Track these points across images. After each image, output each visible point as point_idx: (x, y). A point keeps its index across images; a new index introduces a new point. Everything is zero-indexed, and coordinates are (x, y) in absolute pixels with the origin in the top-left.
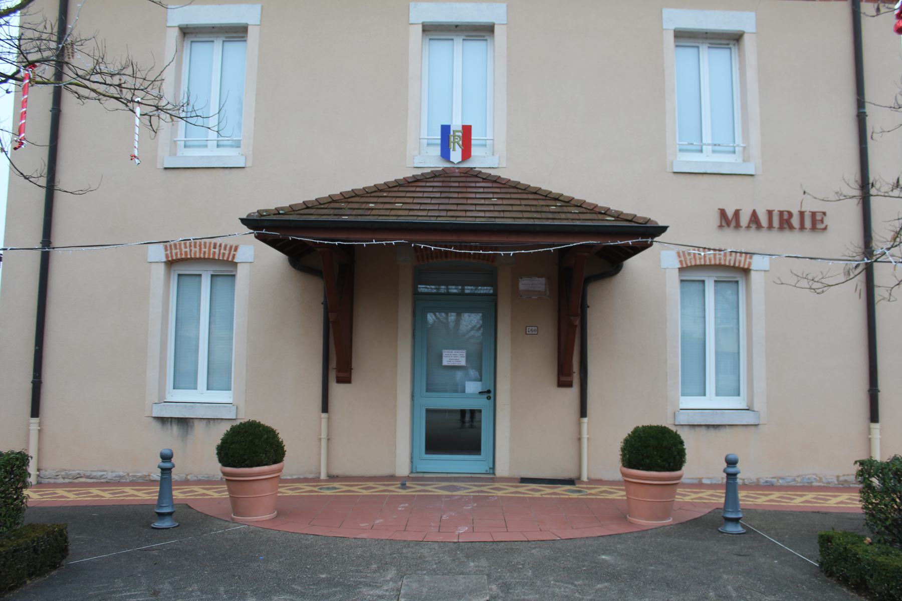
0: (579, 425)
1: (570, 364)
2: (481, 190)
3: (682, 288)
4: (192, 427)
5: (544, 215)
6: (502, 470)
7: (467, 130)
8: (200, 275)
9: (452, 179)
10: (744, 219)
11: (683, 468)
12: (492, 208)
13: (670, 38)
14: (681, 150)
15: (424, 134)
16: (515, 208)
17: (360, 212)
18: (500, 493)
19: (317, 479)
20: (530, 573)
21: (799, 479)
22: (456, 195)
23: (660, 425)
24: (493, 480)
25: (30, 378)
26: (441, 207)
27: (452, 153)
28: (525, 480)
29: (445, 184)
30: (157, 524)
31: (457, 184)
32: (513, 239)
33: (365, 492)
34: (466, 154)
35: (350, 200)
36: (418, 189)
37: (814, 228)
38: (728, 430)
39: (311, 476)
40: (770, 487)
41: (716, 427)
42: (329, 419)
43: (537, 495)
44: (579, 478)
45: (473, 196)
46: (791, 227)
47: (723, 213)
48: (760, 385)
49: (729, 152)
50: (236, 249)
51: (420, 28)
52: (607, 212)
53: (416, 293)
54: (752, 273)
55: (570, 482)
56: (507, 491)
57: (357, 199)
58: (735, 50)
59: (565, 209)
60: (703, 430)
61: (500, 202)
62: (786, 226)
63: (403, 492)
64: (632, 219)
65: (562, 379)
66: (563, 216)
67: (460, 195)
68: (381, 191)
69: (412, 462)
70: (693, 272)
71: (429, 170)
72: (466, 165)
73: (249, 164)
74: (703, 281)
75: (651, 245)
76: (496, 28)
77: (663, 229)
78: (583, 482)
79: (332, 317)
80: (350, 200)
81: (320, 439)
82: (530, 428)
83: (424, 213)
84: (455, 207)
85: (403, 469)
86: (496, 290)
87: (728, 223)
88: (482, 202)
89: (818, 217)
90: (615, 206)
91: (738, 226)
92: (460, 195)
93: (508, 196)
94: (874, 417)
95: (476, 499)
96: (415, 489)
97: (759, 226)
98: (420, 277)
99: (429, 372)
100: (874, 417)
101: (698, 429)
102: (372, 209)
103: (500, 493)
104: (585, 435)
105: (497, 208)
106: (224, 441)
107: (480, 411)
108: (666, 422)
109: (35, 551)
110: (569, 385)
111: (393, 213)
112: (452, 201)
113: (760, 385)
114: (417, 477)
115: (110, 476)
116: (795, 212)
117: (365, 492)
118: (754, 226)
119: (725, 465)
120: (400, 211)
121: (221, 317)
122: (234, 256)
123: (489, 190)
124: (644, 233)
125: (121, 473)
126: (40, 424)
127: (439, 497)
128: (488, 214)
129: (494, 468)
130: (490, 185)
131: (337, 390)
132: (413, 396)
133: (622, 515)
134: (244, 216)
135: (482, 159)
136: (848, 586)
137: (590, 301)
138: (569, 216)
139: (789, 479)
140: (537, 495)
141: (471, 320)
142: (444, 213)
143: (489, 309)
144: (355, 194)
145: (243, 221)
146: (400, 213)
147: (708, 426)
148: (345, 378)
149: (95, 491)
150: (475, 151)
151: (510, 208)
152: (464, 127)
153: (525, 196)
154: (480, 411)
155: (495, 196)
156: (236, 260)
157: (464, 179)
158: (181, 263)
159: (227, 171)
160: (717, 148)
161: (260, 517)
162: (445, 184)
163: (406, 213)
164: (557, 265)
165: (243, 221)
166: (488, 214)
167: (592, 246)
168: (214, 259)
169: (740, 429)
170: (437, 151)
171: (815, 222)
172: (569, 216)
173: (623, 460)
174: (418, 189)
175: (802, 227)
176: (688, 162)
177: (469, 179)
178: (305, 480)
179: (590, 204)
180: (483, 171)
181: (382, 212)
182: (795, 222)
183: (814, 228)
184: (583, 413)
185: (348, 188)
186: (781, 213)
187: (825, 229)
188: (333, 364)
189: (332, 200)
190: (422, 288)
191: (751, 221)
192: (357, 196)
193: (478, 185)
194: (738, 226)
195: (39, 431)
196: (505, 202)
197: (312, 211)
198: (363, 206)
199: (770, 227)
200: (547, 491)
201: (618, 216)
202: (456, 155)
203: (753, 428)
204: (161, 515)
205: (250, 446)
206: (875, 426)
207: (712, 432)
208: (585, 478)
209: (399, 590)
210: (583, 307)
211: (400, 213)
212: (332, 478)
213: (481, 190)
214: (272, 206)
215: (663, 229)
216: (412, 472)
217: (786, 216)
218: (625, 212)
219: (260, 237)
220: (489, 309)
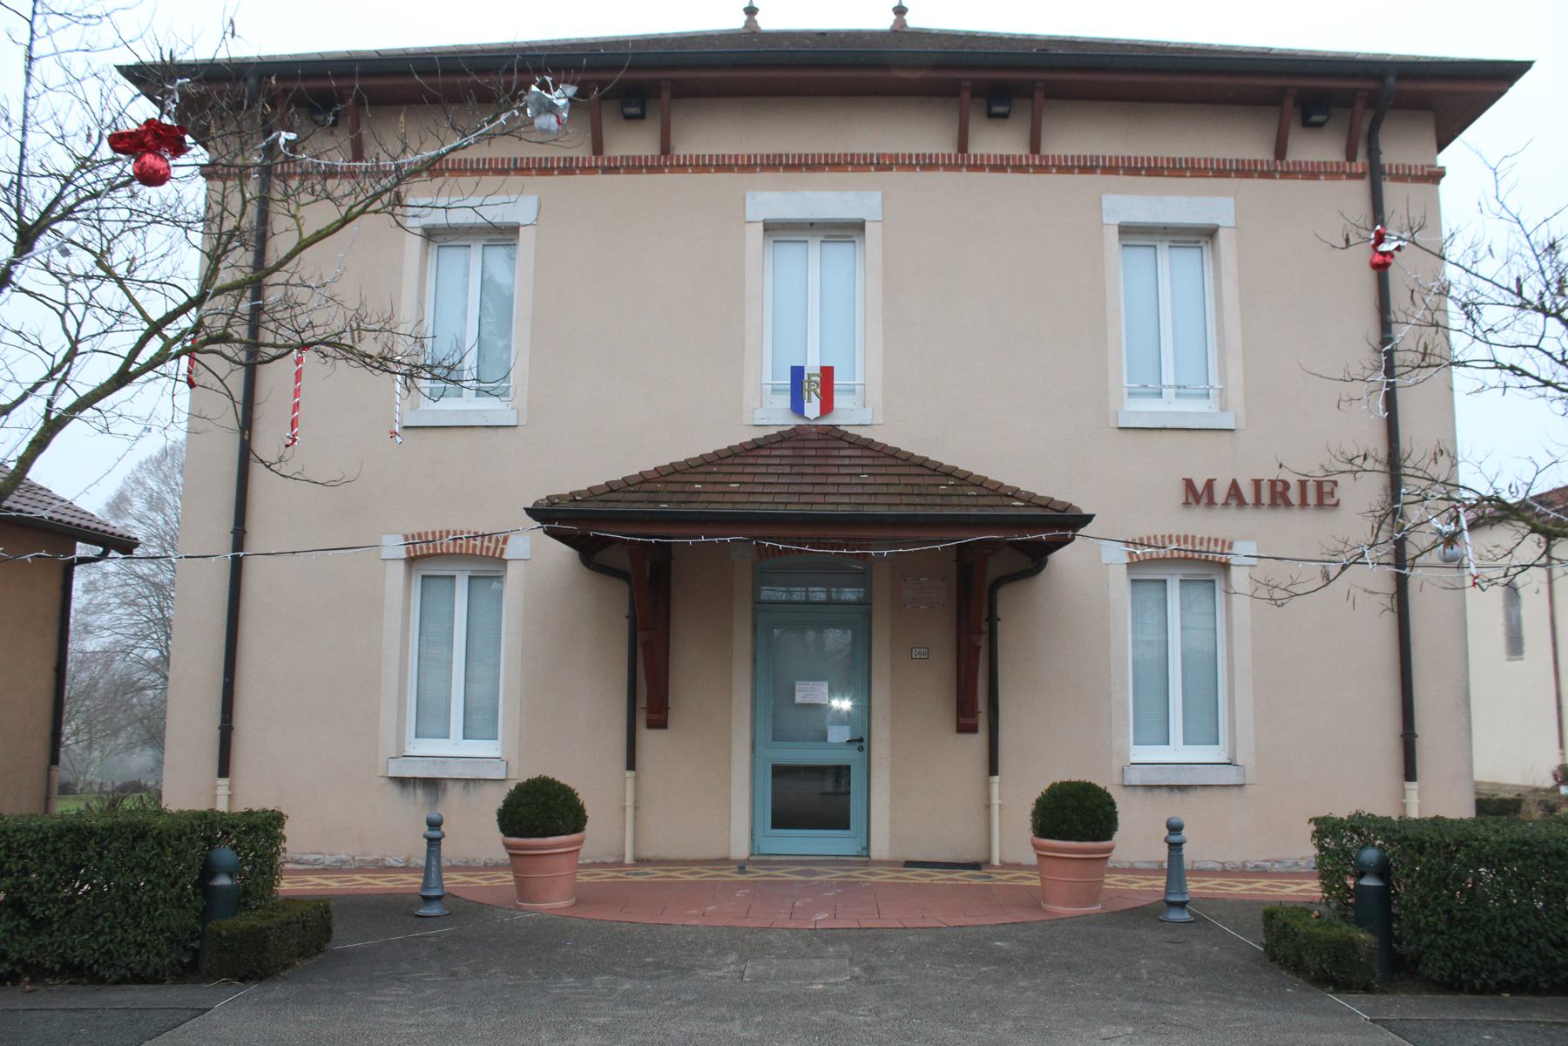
0: (988, 785)
1: (974, 703)
2: (847, 461)
3: (1134, 594)
4: (445, 790)
5: (930, 500)
6: (880, 850)
7: (827, 373)
9: (808, 444)
10: (1220, 493)
11: (1117, 836)
13: (1112, 235)
14: (1131, 394)
16: (892, 490)
18: (873, 879)
19: (620, 864)
20: (902, 957)
21: (1303, 863)
22: (811, 470)
23: (1075, 779)
24: (868, 863)
25: (217, 722)
27: (806, 404)
28: (910, 864)
29: (798, 452)
30: (422, 912)
31: (813, 453)
32: (888, 533)
36: (760, 461)
37: (1320, 504)
38: (1199, 792)
39: (612, 860)
41: (1182, 788)
42: (636, 779)
43: (926, 880)
44: (988, 863)
45: (835, 470)
46: (1288, 504)
47: (1189, 484)
49: (1200, 396)
50: (505, 541)
51: (761, 226)
52: (1015, 493)
53: (757, 602)
54: (1233, 569)
55: (975, 866)
56: (887, 876)
57: (677, 477)
59: (959, 490)
60: (1164, 793)
61: (871, 480)
62: (1279, 501)
63: (741, 877)
64: (1047, 503)
65: (963, 721)
66: (955, 500)
69: (752, 839)
70: (1151, 567)
71: (773, 431)
72: (826, 422)
75: (1072, 539)
78: (993, 867)
79: (1108, 808)
81: (624, 808)
82: (926, 800)
85: (740, 850)
87: (1197, 499)
88: (847, 480)
89: (1327, 488)
90: (1028, 484)
91: (1211, 502)
92: (818, 470)
93: (883, 471)
94: (1410, 773)
95: (840, 884)
97: (1241, 503)
98: (761, 577)
99: (779, 714)
100: (1410, 773)
101: (1156, 792)
102: (698, 492)
103: (873, 879)
104: (996, 800)
105: (867, 489)
106: (507, 804)
107: (848, 768)
109: (304, 927)
110: (973, 729)
111: (727, 498)
115: (328, 860)
116: (1293, 480)
118: (1233, 502)
120: (736, 496)
123: (858, 461)
124: (1066, 523)
125: (343, 857)
128: (854, 499)
130: (858, 452)
131: (649, 739)
132: (753, 747)
133: (1035, 901)
135: (849, 413)
136: (1287, 968)
138: (964, 500)
139: (1289, 863)
140: (926, 880)
141: (837, 639)
142: (795, 499)
143: (860, 620)
144: (674, 469)
145: (530, 512)
146: (737, 498)
147: (1171, 788)
148: (659, 721)
150: (839, 401)
152: (822, 368)
153: (906, 470)
154: (848, 768)
155: (867, 470)
156: (505, 556)
157: (822, 444)
158: (427, 559)
160: (1182, 391)
162: (798, 452)
163: (743, 498)
164: (955, 565)
165: (530, 512)
166: (854, 499)
167: (995, 541)
169: (1216, 791)
170: (785, 401)
171: (1321, 495)
172: (964, 500)
173: (1034, 827)
174: (760, 461)
175: (1304, 503)
177: (830, 444)
178: (603, 865)
179: (994, 482)
180: (851, 431)
181: (713, 498)
182: (1294, 495)
183: (1320, 504)
184: (993, 769)
185: (665, 461)
186: (1273, 483)
187: (1337, 504)
188: (642, 701)
189: (644, 478)
190: (768, 593)
191: (1229, 495)
193: (843, 453)
196: (879, 480)
198: (687, 488)
199: (1258, 502)
200: (940, 876)
201: (1030, 500)
202: (812, 408)
203: (1236, 790)
204: (428, 900)
205: (540, 810)
206: (1412, 787)
207: (1177, 795)
208: (996, 862)
209: (743, 972)
210: (993, 619)
211: (737, 498)
212: (640, 861)
213: (847, 461)
214: (565, 490)
217: (1280, 488)
219: (551, 533)
220: (860, 620)
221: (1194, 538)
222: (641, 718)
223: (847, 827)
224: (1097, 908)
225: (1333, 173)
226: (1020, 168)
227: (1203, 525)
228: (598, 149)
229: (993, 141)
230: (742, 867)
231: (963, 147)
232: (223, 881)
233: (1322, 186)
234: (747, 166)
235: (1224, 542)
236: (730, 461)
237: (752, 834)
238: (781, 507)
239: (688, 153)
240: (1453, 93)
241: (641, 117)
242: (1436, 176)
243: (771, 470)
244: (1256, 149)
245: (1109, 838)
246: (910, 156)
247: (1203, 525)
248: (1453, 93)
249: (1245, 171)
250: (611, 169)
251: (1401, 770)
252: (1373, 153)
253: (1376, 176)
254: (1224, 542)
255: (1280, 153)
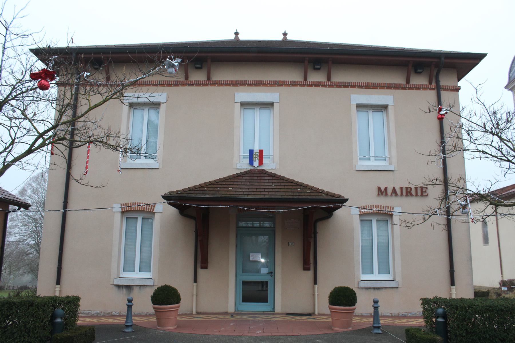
0: (314, 288)
1: (309, 261)
2: (267, 181)
3: (361, 224)
4: (133, 289)
6: (278, 309)
7: (261, 152)
8: (137, 218)
9: (255, 175)
10: (390, 192)
11: (356, 305)
12: (272, 190)
13: (354, 107)
14: (360, 159)
15: (241, 154)
17: (214, 192)
18: (276, 319)
19: (191, 314)
21: (418, 313)
23: (343, 286)
24: (274, 314)
25: (56, 266)
26: (250, 190)
27: (254, 162)
28: (288, 314)
32: (281, 205)
33: (215, 319)
34: (261, 163)
35: (209, 186)
36: (239, 181)
37: (422, 195)
38: (384, 290)
39: (188, 313)
40: (404, 317)
42: (197, 286)
43: (293, 320)
44: (314, 314)
45: (263, 184)
46: (411, 195)
47: (379, 188)
48: (399, 269)
50: (154, 206)
51: (240, 104)
52: (323, 192)
53: (238, 227)
54: (394, 216)
55: (310, 315)
56: (280, 318)
57: (212, 186)
58: (385, 113)
59: (304, 191)
60: (372, 290)
61: (276, 187)
64: (333, 195)
66: (303, 194)
67: (258, 184)
68: (222, 181)
69: (236, 306)
70: (367, 216)
71: (243, 171)
73: (161, 167)
74: (371, 220)
75: (341, 207)
76: (275, 104)
77: (347, 200)
78: (316, 315)
80: (209, 186)
82: (293, 293)
83: (242, 193)
84: (255, 190)
85: (231, 309)
86: (274, 224)
87: (382, 194)
88: (268, 187)
89: (424, 190)
90: (326, 189)
91: (386, 195)
92: (258, 184)
93: (279, 184)
94: (452, 283)
95: (265, 321)
96: (237, 318)
97: (396, 195)
99: (244, 264)
100: (452, 283)
101: (369, 290)
102: (219, 191)
103: (276, 319)
104: (316, 293)
105: (274, 190)
106: (155, 294)
108: (352, 286)
110: (309, 269)
112: (254, 187)
113: (399, 269)
114: (237, 312)
115: (93, 313)
116: (413, 187)
117: (215, 319)
118: (394, 194)
119: (373, 303)
120: (232, 192)
121: (146, 239)
122: (153, 209)
123: (271, 181)
125: (98, 312)
126: (60, 288)
127: (249, 320)
128: (270, 194)
129: (274, 309)
130: (271, 178)
131: (201, 272)
133: (330, 327)
134: (163, 195)
135: (268, 165)
137: (317, 231)
138: (306, 194)
139: (413, 313)
140: (293, 320)
141: (263, 239)
142: (250, 193)
143: (272, 233)
146: (231, 193)
147: (374, 288)
148: (205, 266)
149: (88, 319)
150: (265, 161)
151: (279, 190)
152: (259, 150)
153: (287, 184)
158: (129, 212)
159: (150, 170)
161: (171, 328)
165: (164, 197)
168: (144, 211)
170: (247, 161)
172: (306, 194)
174: (239, 181)
175: (417, 195)
176: (363, 165)
177: (262, 175)
178: (186, 314)
180: (269, 171)
181: (223, 193)
182: (413, 192)
183: (422, 195)
184: (315, 282)
186: (407, 188)
187: (427, 195)
188: (199, 260)
189: (201, 186)
192: (212, 184)
193: (266, 178)
194: (386, 195)
195: (60, 291)
196: (278, 187)
197: (192, 192)
198: (215, 189)
199: (402, 194)
200: (298, 318)
201: (328, 194)
202: (256, 163)
203: (395, 289)
205: (165, 296)
206: (453, 288)
210: (315, 233)
211: (231, 193)
212: (198, 313)
213: (267, 181)
215: (347, 200)
216: (235, 311)
217: (409, 190)
218: (331, 192)
220: (272, 233)
221: (381, 206)
222: (199, 265)
223: (267, 302)
224: (350, 329)
225: (425, 88)
226: (324, 86)
227: (384, 202)
228: (187, 78)
229: (315, 77)
230: (232, 315)
231: (305, 79)
232: (59, 320)
233: (421, 92)
234: (235, 84)
235: (391, 207)
236: (229, 180)
237: (236, 304)
238: (246, 196)
239: (216, 80)
240: (463, 63)
241: (201, 68)
242: (458, 89)
243: (243, 183)
244: (400, 80)
245: (354, 305)
246: (288, 81)
247: (384, 202)
248: (463, 63)
249: (397, 87)
250: (191, 85)
251: (450, 282)
252: (438, 82)
253: (438, 89)
254: (391, 207)
255: (408, 81)
